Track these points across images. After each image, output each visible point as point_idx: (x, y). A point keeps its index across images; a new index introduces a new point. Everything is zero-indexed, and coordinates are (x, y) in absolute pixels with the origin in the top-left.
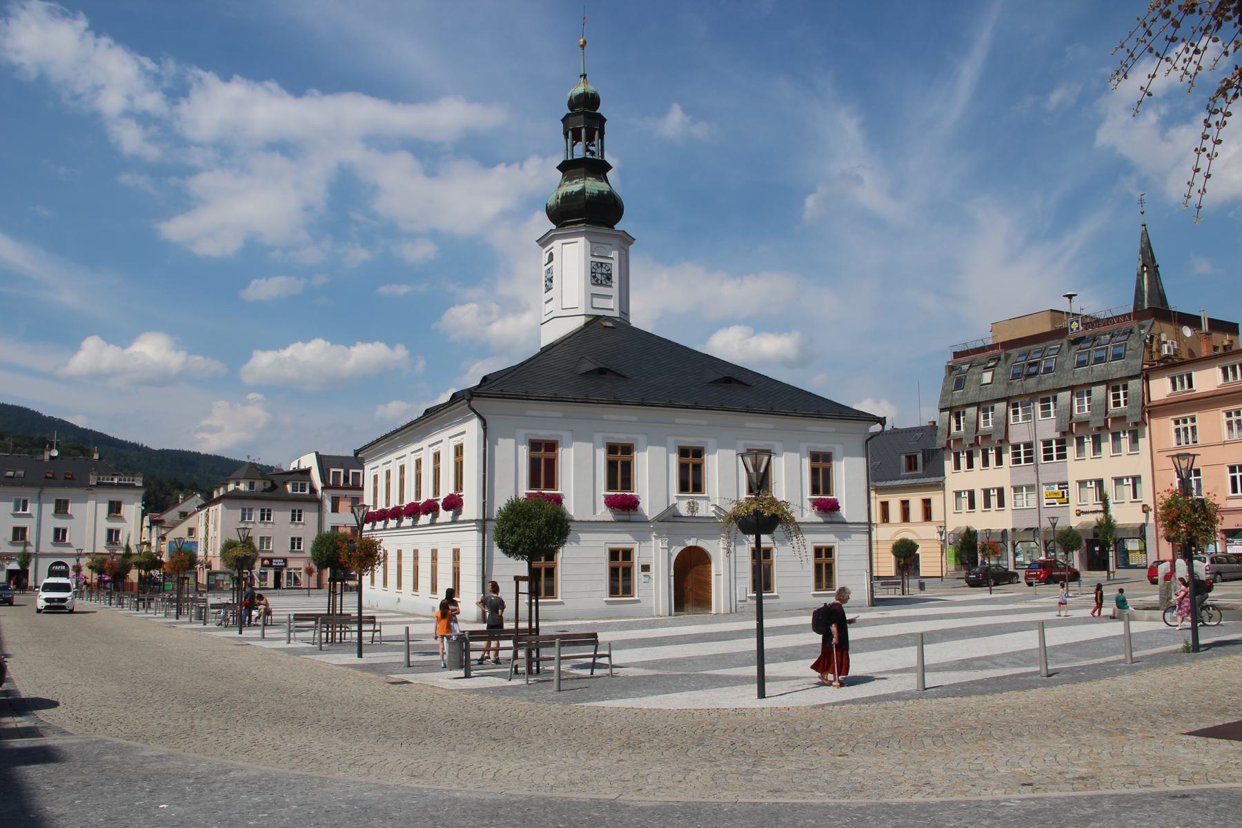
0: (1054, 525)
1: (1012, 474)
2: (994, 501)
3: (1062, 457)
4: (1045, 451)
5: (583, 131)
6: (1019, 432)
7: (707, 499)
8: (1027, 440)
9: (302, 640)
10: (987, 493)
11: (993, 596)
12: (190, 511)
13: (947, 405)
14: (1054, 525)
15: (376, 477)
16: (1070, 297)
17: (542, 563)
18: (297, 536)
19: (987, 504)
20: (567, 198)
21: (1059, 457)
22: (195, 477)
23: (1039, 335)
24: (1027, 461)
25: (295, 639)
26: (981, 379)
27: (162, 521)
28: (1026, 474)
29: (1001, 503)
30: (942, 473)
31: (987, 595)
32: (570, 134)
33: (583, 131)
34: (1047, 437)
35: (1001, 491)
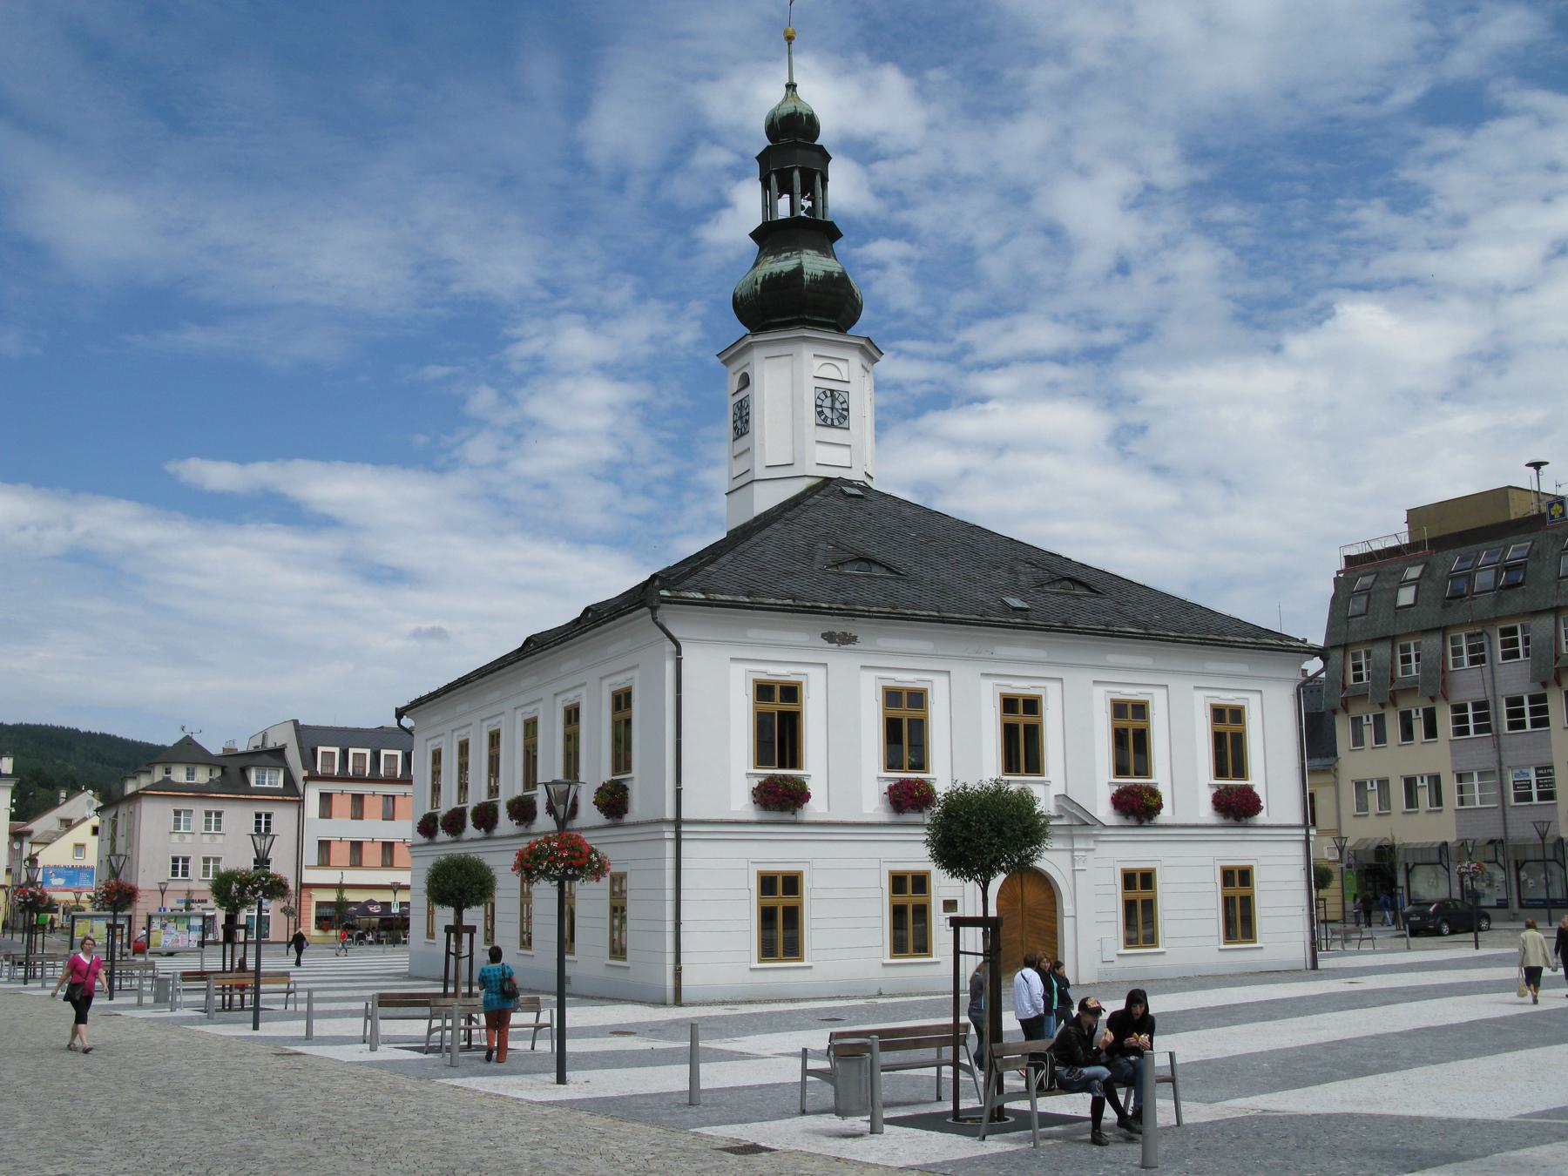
0: (1543, 837)
1: (1454, 753)
2: (1424, 796)
3: (1541, 722)
4: (1511, 714)
5: (796, 174)
6: (1469, 684)
7: (1046, 783)
8: (1480, 697)
9: (188, 1005)
10: (1410, 783)
11: (1483, 952)
12: (76, 817)
13: (1341, 640)
14: (1543, 837)
15: (437, 756)
16: (1537, 465)
17: (473, 916)
18: (180, 854)
19: (1411, 801)
20: (774, 283)
21: (1535, 724)
22: (71, 767)
23: (1493, 527)
24: (1478, 730)
25: (389, 1040)
26: (123, 788)
27: (29, 833)
28: (1479, 751)
29: (1438, 799)
30: (1333, 753)
31: (1469, 952)
32: (773, 178)
33: (796, 174)
34: (1513, 692)
35: (1435, 780)
